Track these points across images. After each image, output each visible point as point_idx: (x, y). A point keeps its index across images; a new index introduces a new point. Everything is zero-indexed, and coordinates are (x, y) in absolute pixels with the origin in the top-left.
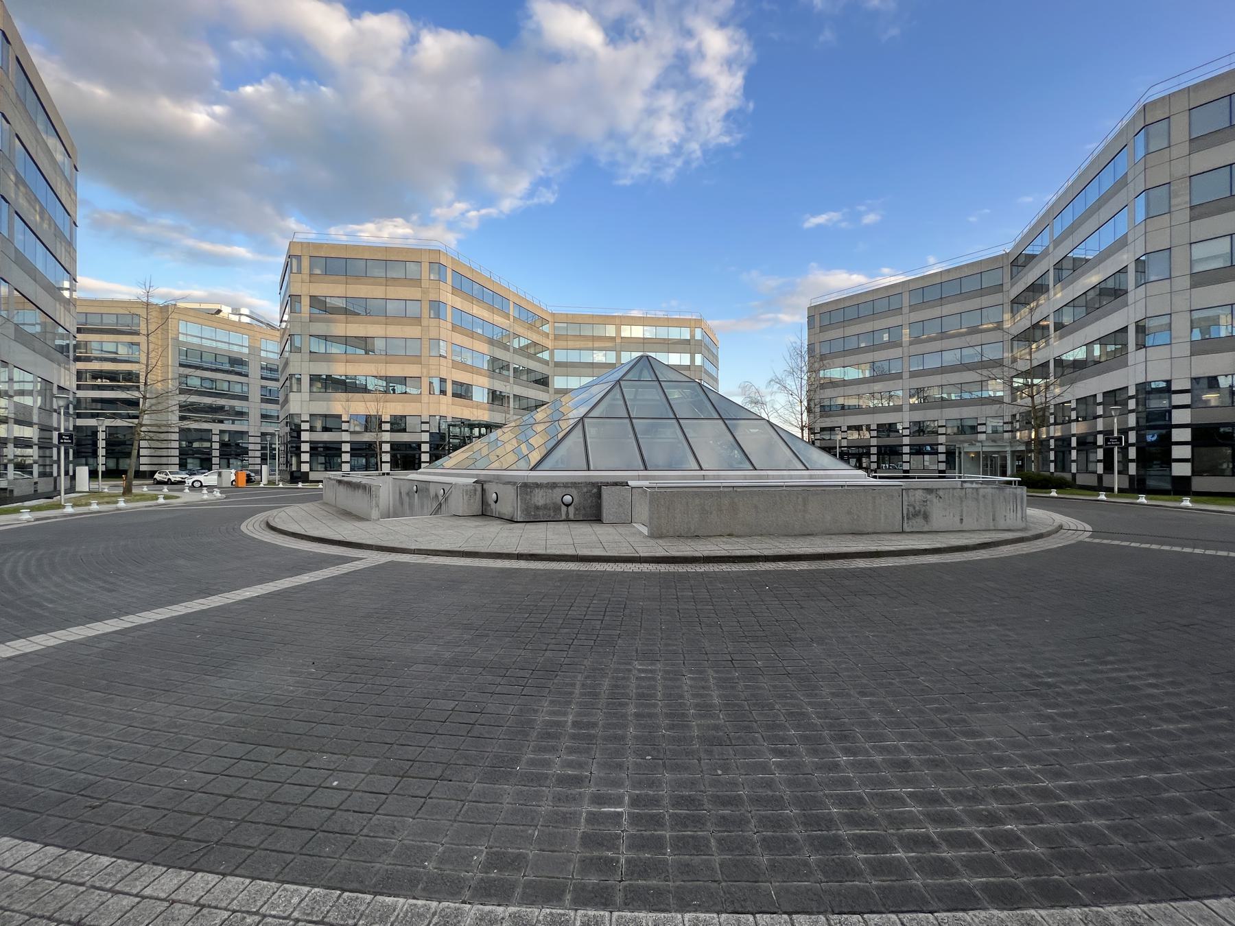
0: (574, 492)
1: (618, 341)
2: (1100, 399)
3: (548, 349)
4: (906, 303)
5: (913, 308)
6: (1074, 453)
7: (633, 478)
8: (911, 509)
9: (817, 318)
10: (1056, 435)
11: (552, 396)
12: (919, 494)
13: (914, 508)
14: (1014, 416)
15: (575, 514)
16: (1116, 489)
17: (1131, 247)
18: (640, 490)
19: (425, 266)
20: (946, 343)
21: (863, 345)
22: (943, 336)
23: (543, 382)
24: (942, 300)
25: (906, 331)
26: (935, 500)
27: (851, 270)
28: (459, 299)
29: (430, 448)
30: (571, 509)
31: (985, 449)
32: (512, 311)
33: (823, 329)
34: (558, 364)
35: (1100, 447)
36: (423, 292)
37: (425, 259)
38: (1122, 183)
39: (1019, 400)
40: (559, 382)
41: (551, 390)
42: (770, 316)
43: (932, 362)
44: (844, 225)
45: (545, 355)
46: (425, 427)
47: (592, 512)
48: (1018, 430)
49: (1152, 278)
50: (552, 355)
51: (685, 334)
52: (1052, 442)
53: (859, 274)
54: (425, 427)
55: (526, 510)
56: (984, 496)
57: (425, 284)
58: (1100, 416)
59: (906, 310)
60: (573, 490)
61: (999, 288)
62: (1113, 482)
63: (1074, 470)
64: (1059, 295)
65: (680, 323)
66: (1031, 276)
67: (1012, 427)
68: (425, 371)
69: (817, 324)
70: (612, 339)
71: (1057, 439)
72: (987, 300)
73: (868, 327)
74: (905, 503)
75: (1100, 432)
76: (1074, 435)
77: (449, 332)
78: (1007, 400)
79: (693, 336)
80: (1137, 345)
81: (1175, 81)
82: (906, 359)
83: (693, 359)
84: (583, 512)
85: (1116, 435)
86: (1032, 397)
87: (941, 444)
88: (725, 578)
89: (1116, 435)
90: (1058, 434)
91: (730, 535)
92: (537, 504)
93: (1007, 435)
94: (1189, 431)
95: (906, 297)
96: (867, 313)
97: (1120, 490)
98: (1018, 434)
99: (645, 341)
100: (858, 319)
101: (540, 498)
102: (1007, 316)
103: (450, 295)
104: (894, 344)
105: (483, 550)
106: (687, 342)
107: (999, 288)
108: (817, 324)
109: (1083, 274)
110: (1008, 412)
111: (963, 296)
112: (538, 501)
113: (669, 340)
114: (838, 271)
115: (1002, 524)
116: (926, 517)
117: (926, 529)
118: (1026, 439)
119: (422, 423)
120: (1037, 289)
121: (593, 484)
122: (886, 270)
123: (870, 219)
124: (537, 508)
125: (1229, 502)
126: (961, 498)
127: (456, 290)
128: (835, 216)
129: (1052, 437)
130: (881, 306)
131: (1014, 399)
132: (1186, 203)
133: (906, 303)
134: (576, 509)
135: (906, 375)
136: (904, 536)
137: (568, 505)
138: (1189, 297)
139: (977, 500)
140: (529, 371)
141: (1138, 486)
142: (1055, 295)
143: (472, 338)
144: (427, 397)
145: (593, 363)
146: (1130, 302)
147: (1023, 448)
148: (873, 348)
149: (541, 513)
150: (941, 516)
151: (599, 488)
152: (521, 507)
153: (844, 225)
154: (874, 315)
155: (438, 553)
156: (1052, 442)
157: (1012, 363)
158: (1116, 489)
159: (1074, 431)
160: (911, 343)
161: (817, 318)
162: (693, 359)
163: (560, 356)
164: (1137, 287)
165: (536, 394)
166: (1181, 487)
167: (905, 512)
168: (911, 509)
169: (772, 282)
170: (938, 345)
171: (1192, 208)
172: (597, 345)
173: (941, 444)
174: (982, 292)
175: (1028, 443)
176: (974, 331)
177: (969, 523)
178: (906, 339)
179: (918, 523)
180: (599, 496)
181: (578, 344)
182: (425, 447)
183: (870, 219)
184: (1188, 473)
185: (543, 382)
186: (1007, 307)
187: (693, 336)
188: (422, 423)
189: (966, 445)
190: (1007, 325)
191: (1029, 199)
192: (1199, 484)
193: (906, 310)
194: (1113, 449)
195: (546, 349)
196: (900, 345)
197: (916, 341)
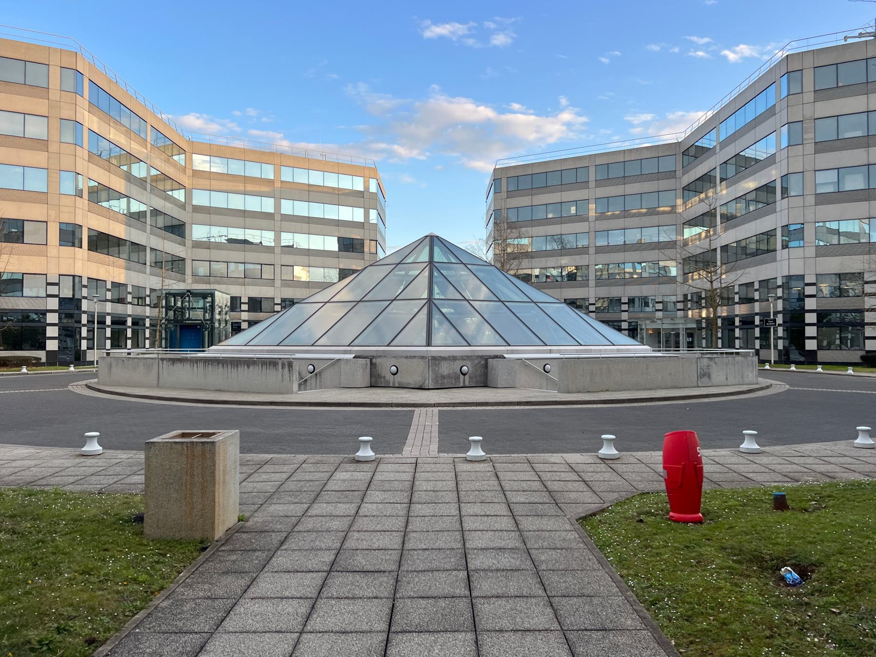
0: (469, 363)
1: (278, 185)
2: (756, 286)
3: (185, 187)
4: (592, 177)
5: (599, 183)
6: (737, 331)
7: (508, 352)
8: (702, 371)
9: (504, 181)
10: (723, 315)
11: (189, 251)
12: (706, 360)
13: (703, 370)
14: (685, 296)
15: (469, 382)
16: (773, 362)
17: (778, 165)
18: (520, 361)
19: (55, 72)
20: (629, 222)
21: (550, 216)
22: (625, 214)
23: (177, 229)
24: (624, 179)
25: (592, 206)
26: (714, 365)
27: (479, 100)
28: (95, 119)
29: (60, 318)
30: (467, 377)
31: (665, 326)
32: (150, 136)
33: (510, 194)
34: (197, 209)
35: (757, 326)
36: (50, 107)
37: (55, 60)
38: (771, 112)
39: (690, 281)
40: (198, 232)
41: (188, 243)
42: (383, 146)
43: (617, 239)
44: (471, 42)
45: (180, 195)
46: (53, 290)
47: (484, 381)
48: (689, 309)
49: (793, 194)
50: (189, 195)
51: (358, 184)
52: (719, 321)
53: (487, 107)
54: (53, 290)
55: (436, 380)
56: (737, 362)
57: (54, 95)
58: (757, 301)
59: (592, 184)
60: (468, 362)
61: (672, 175)
62: (771, 357)
63: (757, 346)
64: (724, 192)
65: (352, 170)
66: (700, 170)
67: (684, 306)
68: (53, 214)
69: (504, 189)
70: (270, 182)
71: (724, 319)
72: (663, 184)
73: (555, 197)
74: (699, 368)
75: (757, 314)
76: (737, 316)
77: (86, 163)
78: (680, 279)
79: (367, 187)
80: (782, 246)
81: (804, 43)
82: (592, 234)
83: (367, 215)
84: (475, 380)
85: (772, 317)
86: (711, 282)
87: (625, 321)
88: (640, 408)
89: (772, 317)
90: (724, 314)
91: (607, 391)
92: (443, 374)
93: (680, 313)
94: (815, 315)
95: (592, 170)
96: (555, 183)
97: (775, 362)
98: (690, 312)
99: (311, 189)
100: (546, 188)
101: (445, 369)
102: (679, 202)
103: (86, 113)
104: (580, 218)
105: (491, 401)
106: (360, 194)
107: (672, 175)
108: (504, 189)
109: (744, 178)
110: (681, 291)
111: (642, 177)
112: (444, 372)
113: (339, 189)
114: (463, 100)
115: (746, 380)
116: (709, 377)
117: (709, 385)
118: (697, 317)
119: (48, 284)
120: (707, 180)
121: (481, 357)
122: (516, 106)
123: (500, 40)
124: (443, 377)
125: (839, 369)
126: (726, 364)
127: (94, 106)
128: (459, 28)
129: (719, 317)
130: (568, 178)
131: (685, 281)
132: (812, 139)
133: (592, 177)
134: (470, 378)
135: (592, 250)
136: (698, 389)
137: (464, 375)
138: (814, 212)
139: (734, 365)
140: (156, 212)
141: (784, 358)
142: (721, 191)
143: (109, 172)
144: (591, 296)
145: (245, 211)
146: (778, 209)
147: (694, 326)
148: (562, 220)
149: (446, 381)
150: (718, 376)
151: (486, 360)
152: (431, 376)
153: (471, 42)
154: (563, 187)
155: (456, 405)
156: (737, 320)
157: (684, 246)
158: (773, 362)
159: (737, 313)
160: (597, 219)
161: (504, 181)
162: (367, 215)
163: (200, 198)
164: (783, 198)
165: (171, 247)
166: (811, 359)
167: (699, 372)
168: (702, 371)
169: (385, 102)
170: (621, 223)
171: (816, 143)
172: (250, 187)
173: (625, 321)
174: (659, 176)
175: (699, 322)
176: (652, 212)
177: (731, 380)
178: (592, 214)
179: (705, 380)
180: (486, 366)
181: (224, 185)
182: (52, 318)
183: (500, 40)
184: (815, 348)
185: (177, 229)
186: (680, 192)
187: (367, 187)
188: (48, 284)
189: (648, 322)
190: (680, 210)
191: (655, 48)
192: (822, 356)
193: (592, 184)
194: (770, 328)
195: (181, 186)
196: (586, 219)
197: (601, 217)
